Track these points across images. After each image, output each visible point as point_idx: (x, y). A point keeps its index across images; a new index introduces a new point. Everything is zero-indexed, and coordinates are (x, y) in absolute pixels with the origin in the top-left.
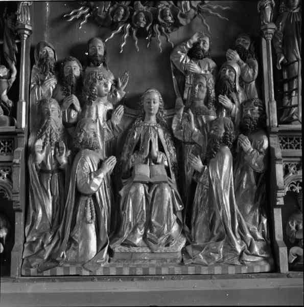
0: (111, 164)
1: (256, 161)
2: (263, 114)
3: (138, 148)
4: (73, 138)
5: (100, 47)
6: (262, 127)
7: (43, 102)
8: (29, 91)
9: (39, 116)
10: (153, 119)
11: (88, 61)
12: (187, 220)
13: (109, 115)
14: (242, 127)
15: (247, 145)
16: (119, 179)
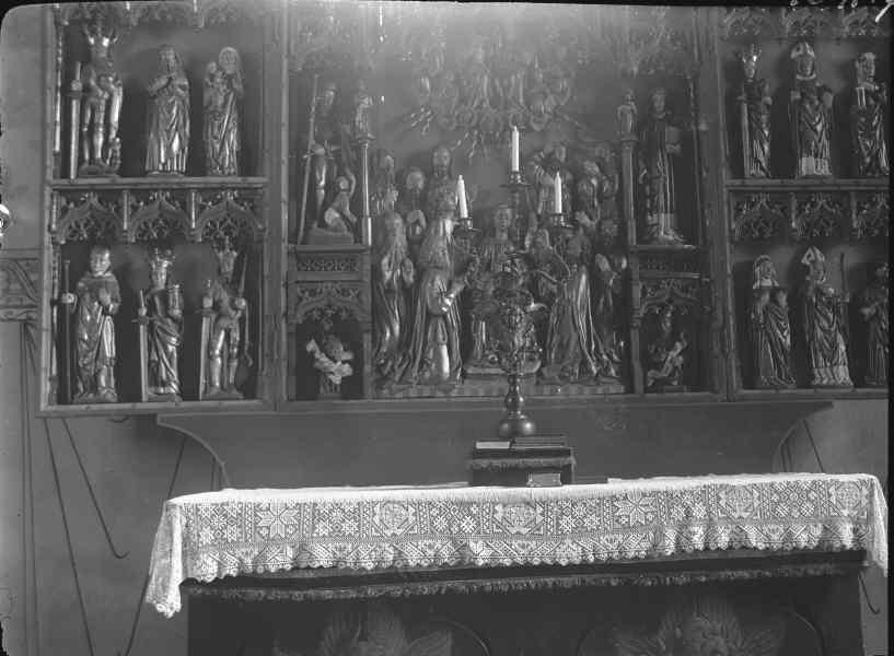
15: (605, 265)
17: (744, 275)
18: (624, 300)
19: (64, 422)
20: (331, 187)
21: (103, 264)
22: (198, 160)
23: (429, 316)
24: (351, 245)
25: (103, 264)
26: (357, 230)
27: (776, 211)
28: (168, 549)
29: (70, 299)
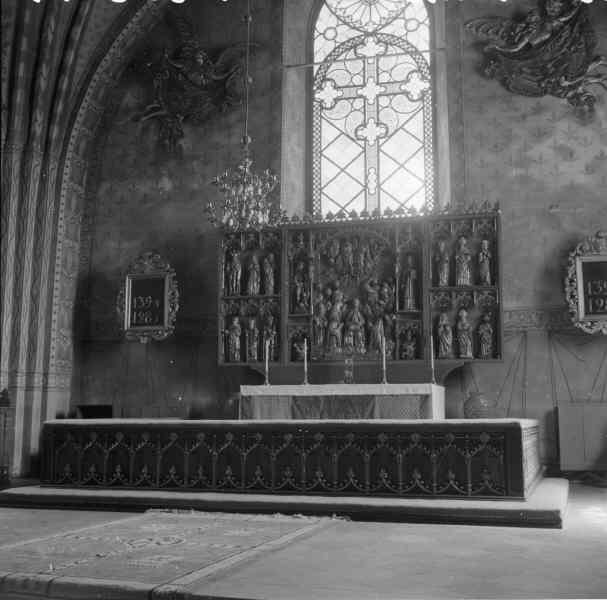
0: (342, 325)
1: (390, 323)
2: (395, 307)
3: (351, 320)
4: (329, 316)
5: (338, 284)
6: (393, 311)
7: (318, 304)
8: (314, 301)
9: (317, 308)
10: (357, 309)
11: (334, 289)
12: (367, 344)
13: (341, 308)
14: (387, 311)
15: (387, 317)
16: (344, 331)
17: (436, 321)
18: (393, 329)
19: (404, 130)
20: (301, 295)
21: (236, 322)
22: (263, 290)
23: (332, 335)
24: (306, 314)
25: (236, 322)
26: (309, 309)
27: (469, 297)
28: (245, 547)
29: (227, 332)
